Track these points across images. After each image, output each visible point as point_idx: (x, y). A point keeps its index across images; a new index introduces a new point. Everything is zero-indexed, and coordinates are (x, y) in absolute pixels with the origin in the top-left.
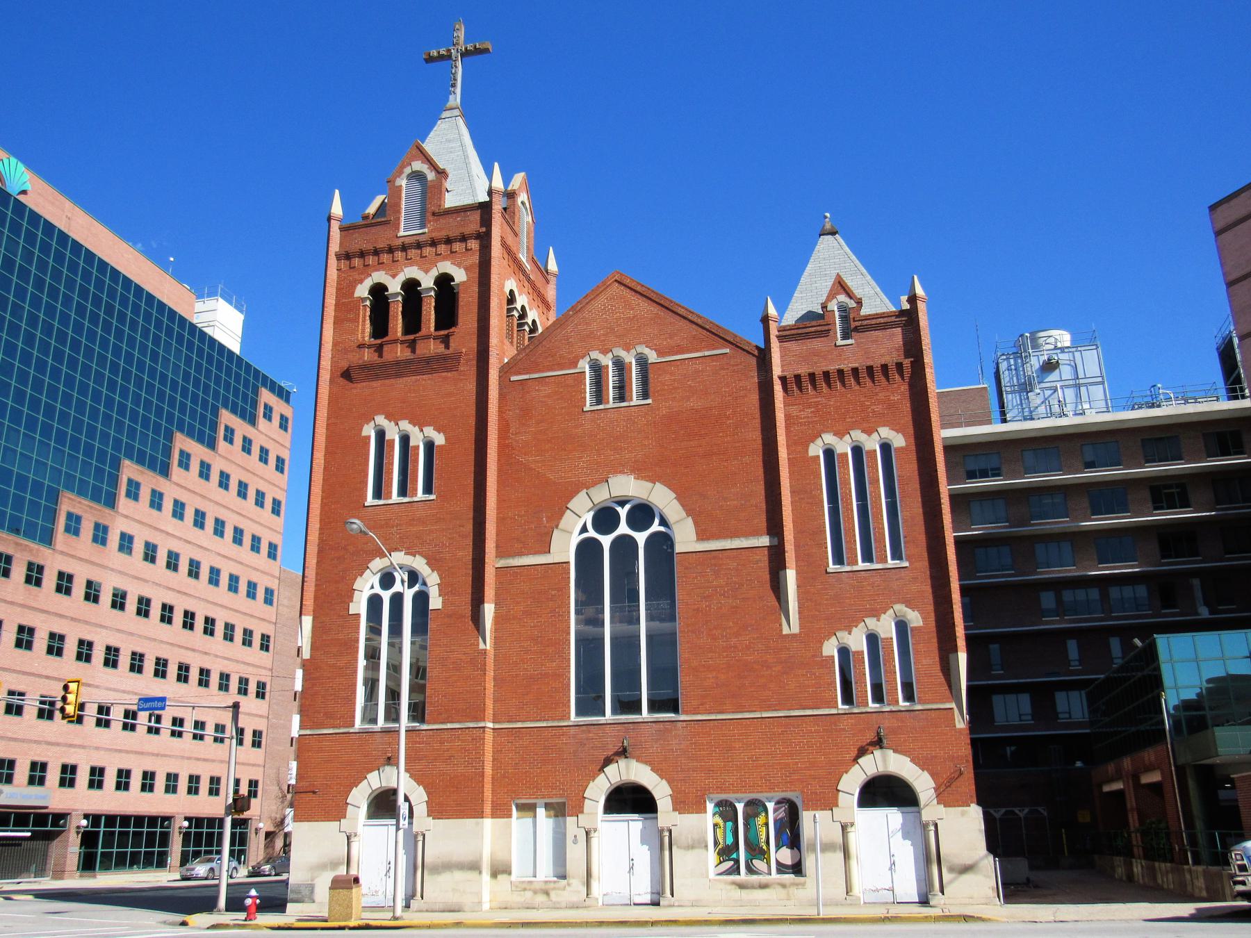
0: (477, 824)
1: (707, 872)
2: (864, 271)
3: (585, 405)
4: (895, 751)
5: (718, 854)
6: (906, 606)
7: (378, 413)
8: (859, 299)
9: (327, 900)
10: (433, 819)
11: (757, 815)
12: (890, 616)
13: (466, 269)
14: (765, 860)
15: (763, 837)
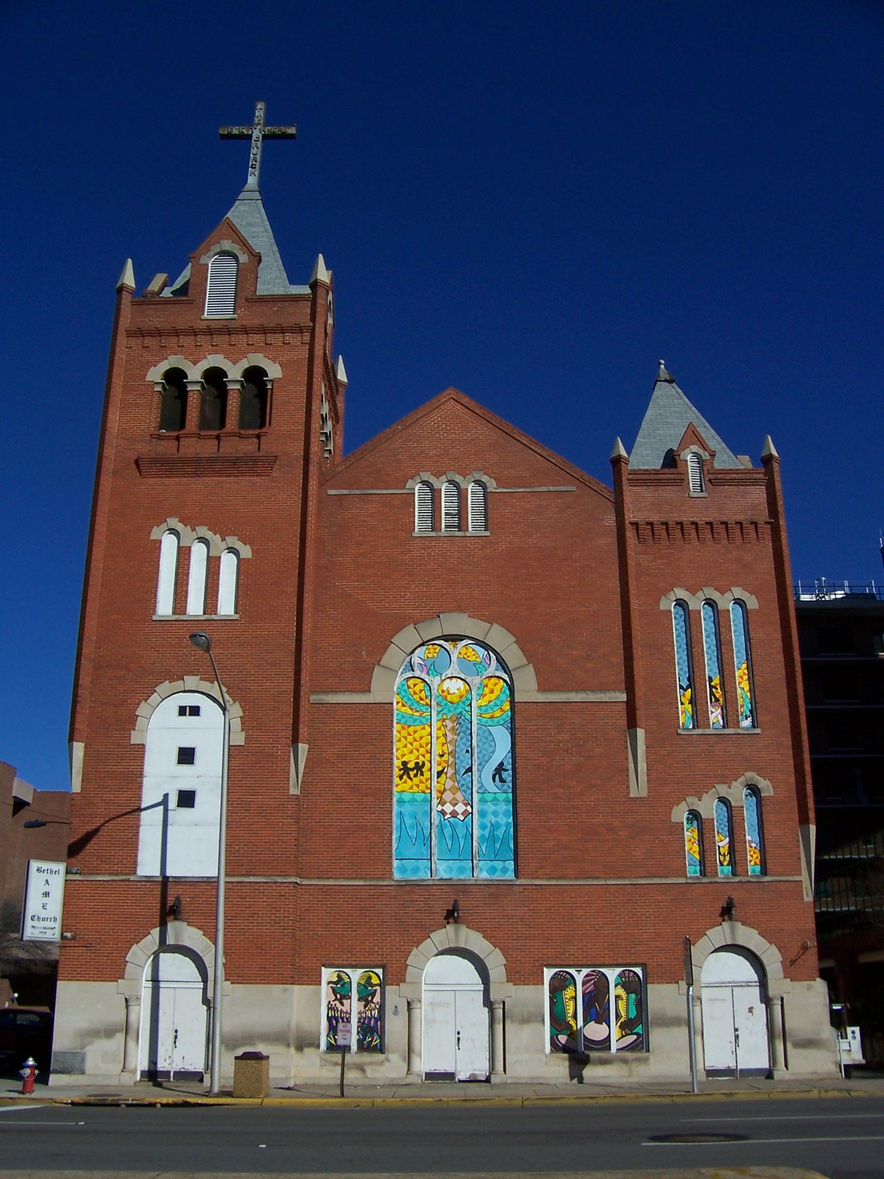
0: (285, 990)
1: (544, 1048)
2: (707, 424)
4: (744, 923)
6: (758, 774)
7: (170, 516)
8: (713, 451)
10: (232, 983)
11: (565, 988)
12: (741, 784)
15: (570, 1012)
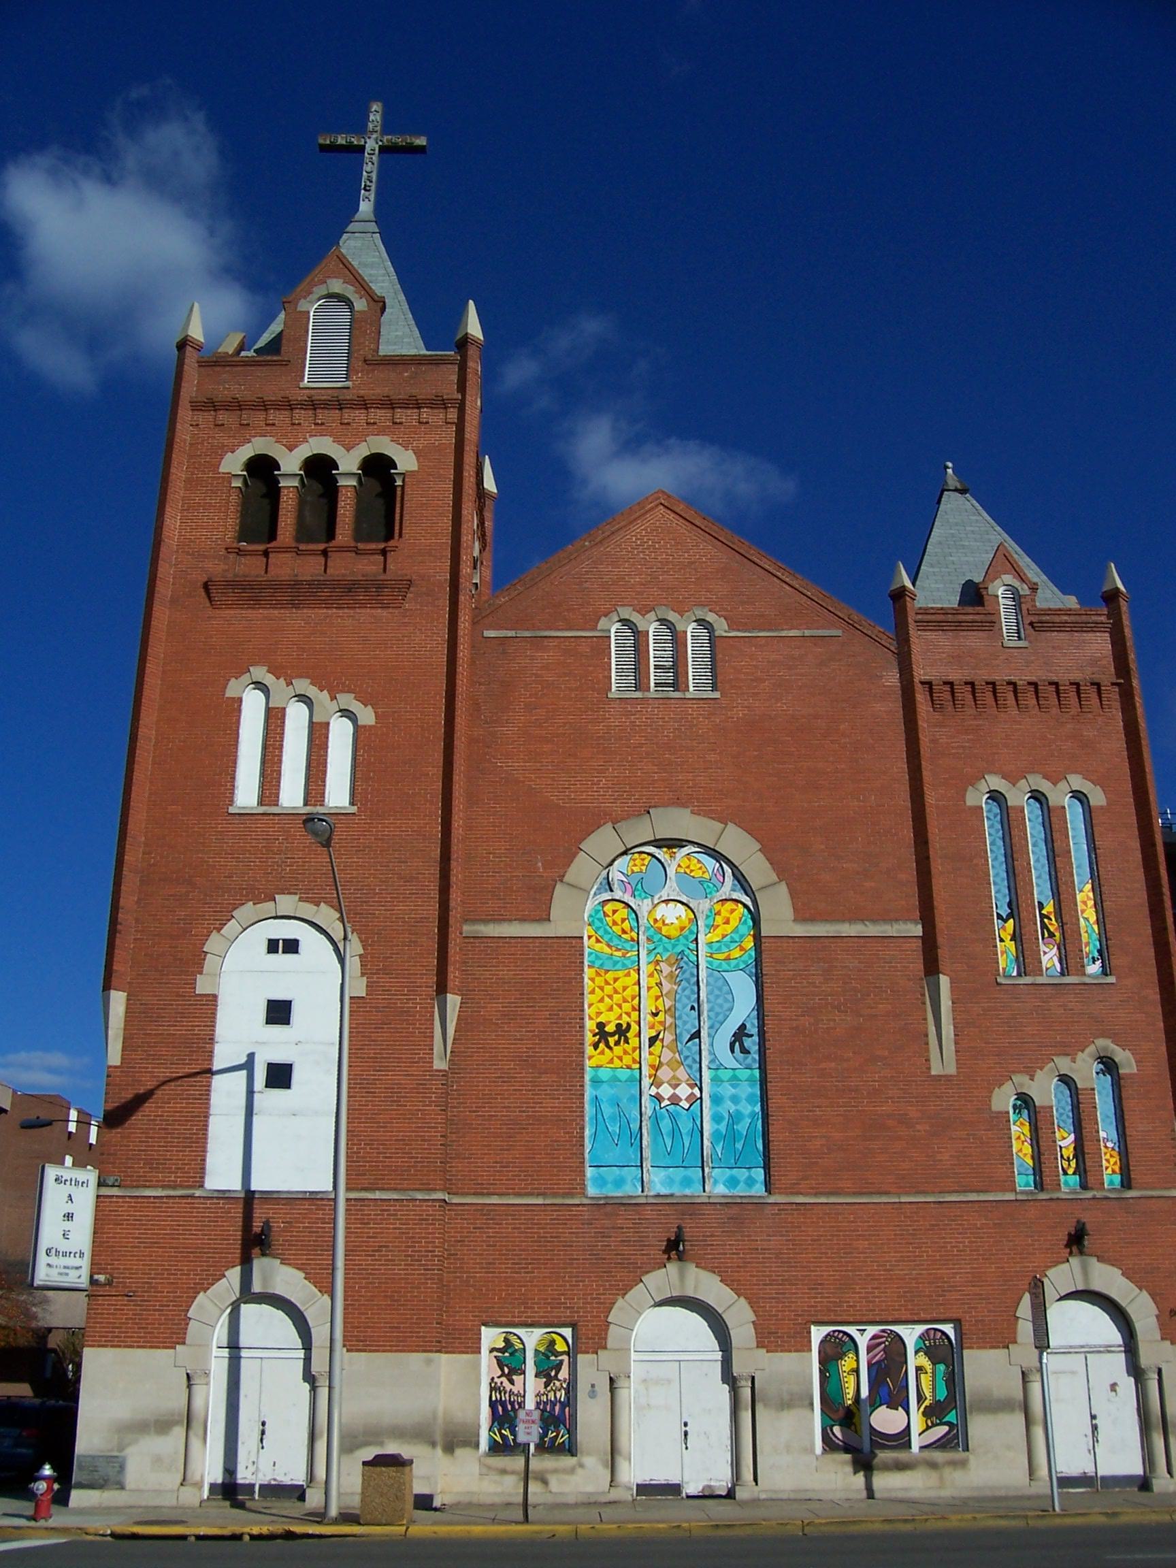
3: (610, 689)
4: (1100, 1259)
5: (924, 1414)
8: (1034, 584)
9: (359, 1490)
11: (841, 1356)
13: (417, 453)
14: (853, 1427)
